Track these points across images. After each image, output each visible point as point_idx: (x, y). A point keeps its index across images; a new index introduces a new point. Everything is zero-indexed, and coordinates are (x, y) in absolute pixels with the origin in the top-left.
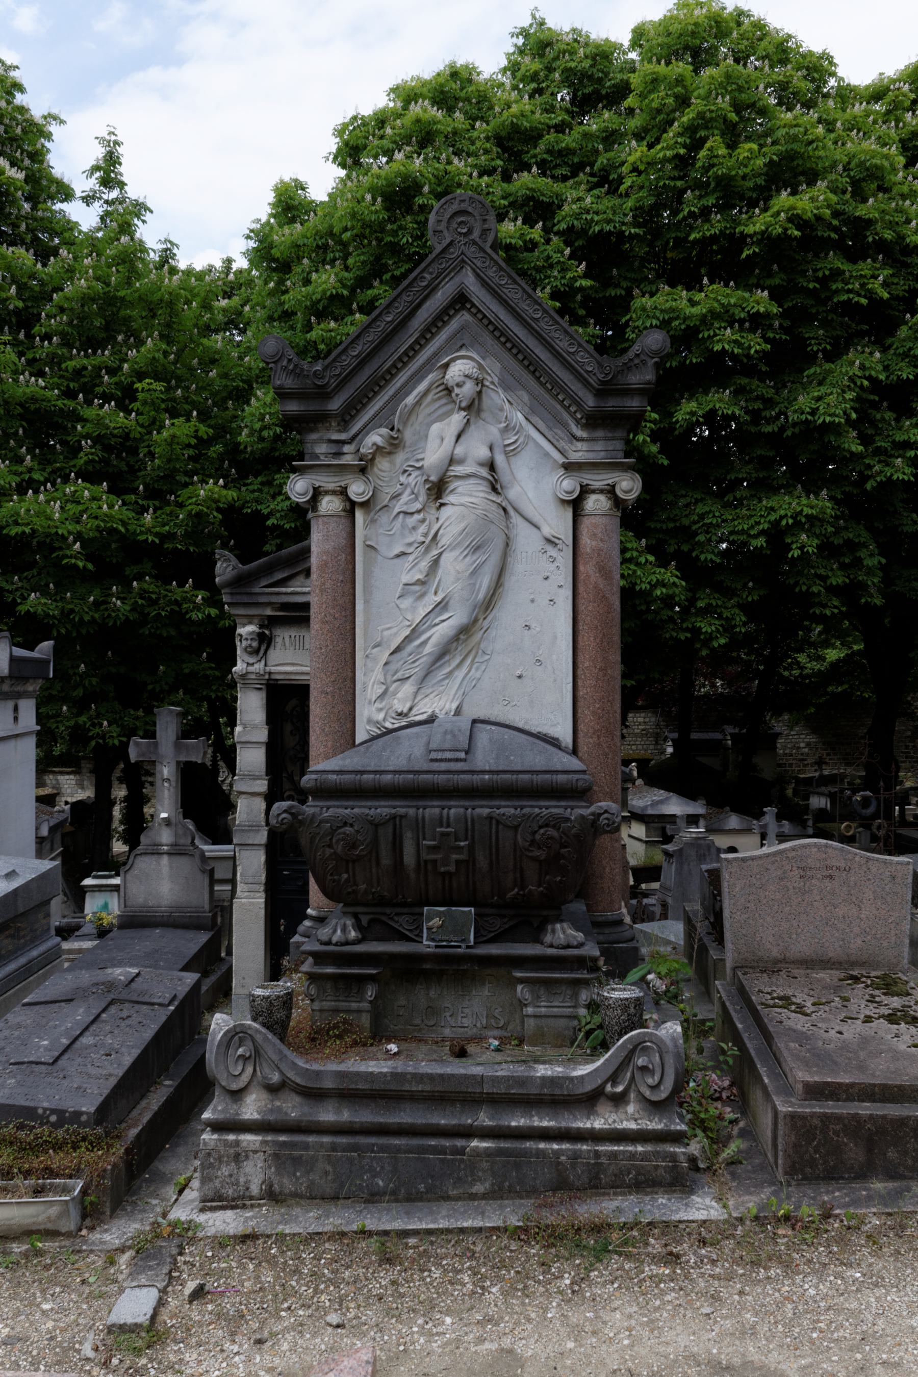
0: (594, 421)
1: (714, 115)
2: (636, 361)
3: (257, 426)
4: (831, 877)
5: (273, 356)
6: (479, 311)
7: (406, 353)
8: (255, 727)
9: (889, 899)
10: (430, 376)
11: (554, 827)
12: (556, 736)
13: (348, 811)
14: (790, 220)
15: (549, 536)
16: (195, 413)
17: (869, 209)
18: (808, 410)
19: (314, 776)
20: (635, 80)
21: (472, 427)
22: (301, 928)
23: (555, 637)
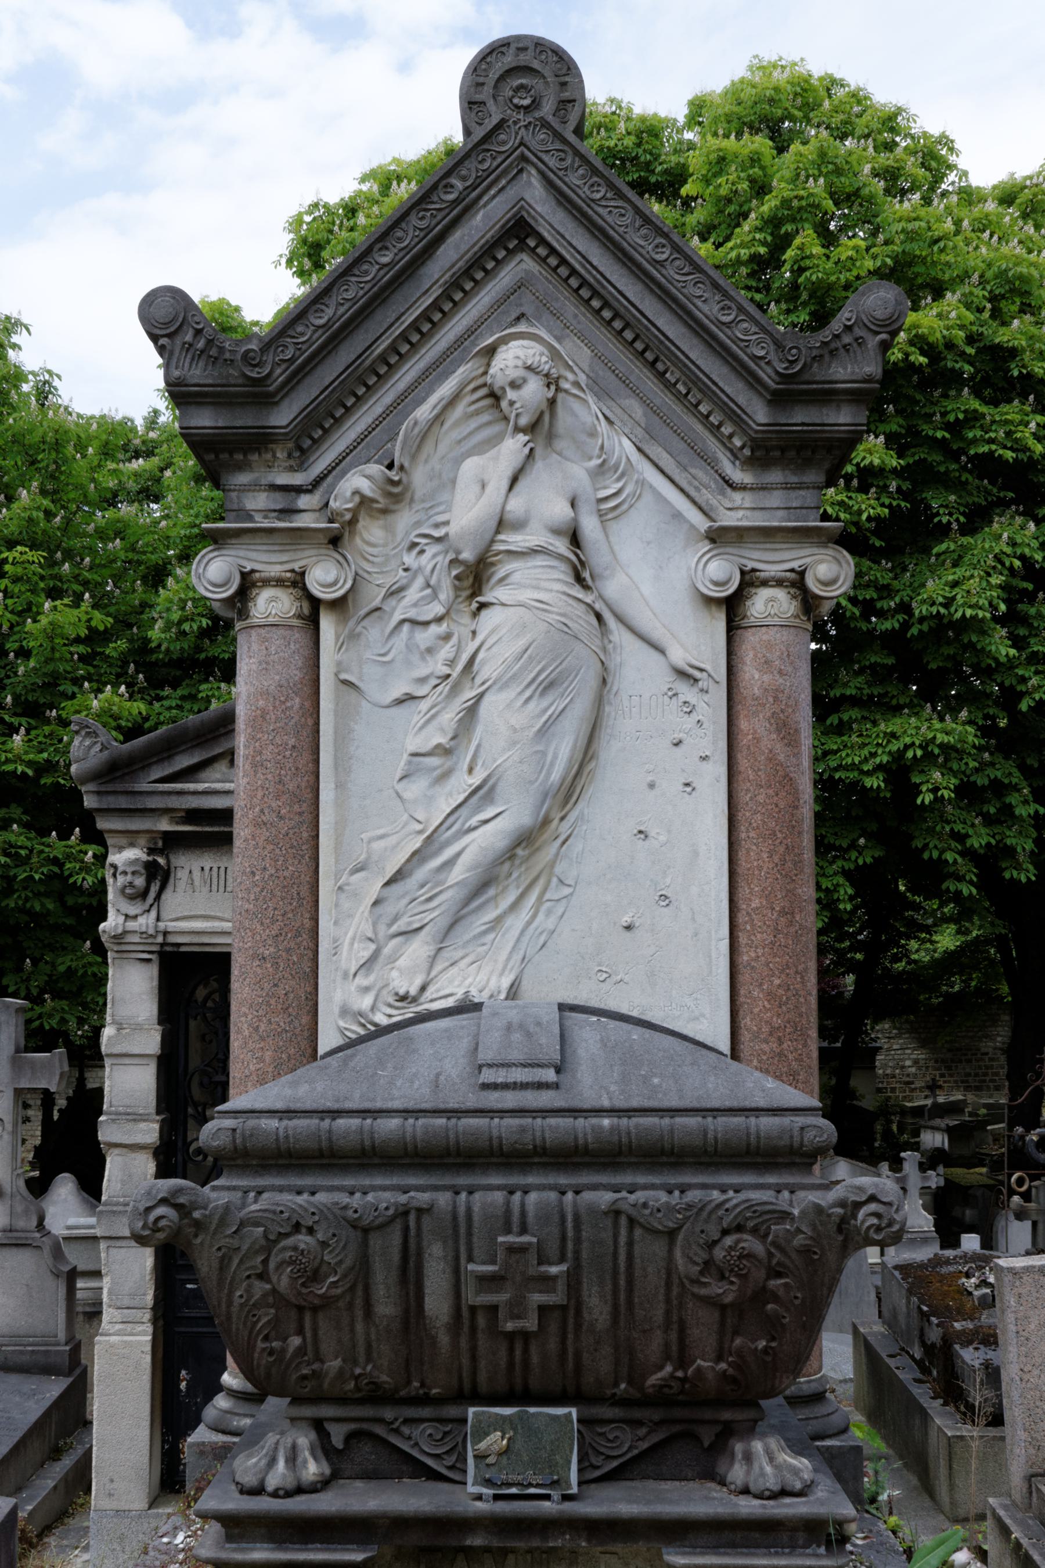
0: (767, 452)
1: (804, 203)
2: (847, 339)
3: (175, 616)
5: (167, 324)
6: (553, 251)
7: (415, 326)
8: (138, 1028)
10: (461, 370)
11: (754, 1231)
13: (302, 1199)
14: (911, 343)
15: (681, 664)
16: (87, 595)
17: (1015, 332)
18: (941, 599)
19: (229, 1123)
20: (695, 161)
21: (539, 465)
22: (210, 1413)
23: (696, 853)
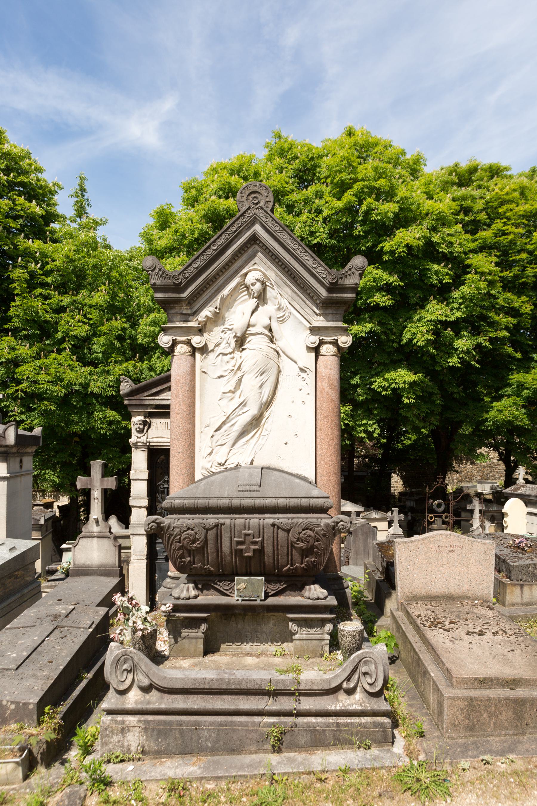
4: (453, 551)
9: (483, 563)
11: (311, 530)
12: (306, 476)
21: (261, 308)
